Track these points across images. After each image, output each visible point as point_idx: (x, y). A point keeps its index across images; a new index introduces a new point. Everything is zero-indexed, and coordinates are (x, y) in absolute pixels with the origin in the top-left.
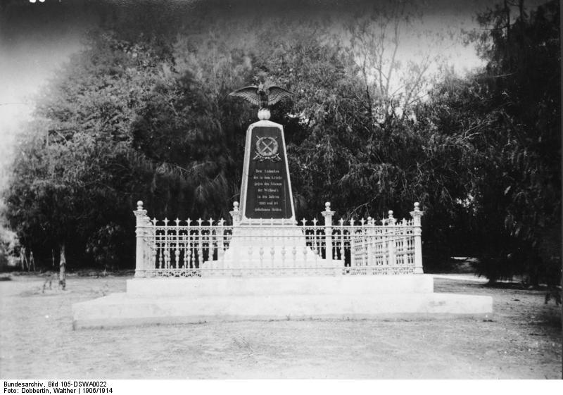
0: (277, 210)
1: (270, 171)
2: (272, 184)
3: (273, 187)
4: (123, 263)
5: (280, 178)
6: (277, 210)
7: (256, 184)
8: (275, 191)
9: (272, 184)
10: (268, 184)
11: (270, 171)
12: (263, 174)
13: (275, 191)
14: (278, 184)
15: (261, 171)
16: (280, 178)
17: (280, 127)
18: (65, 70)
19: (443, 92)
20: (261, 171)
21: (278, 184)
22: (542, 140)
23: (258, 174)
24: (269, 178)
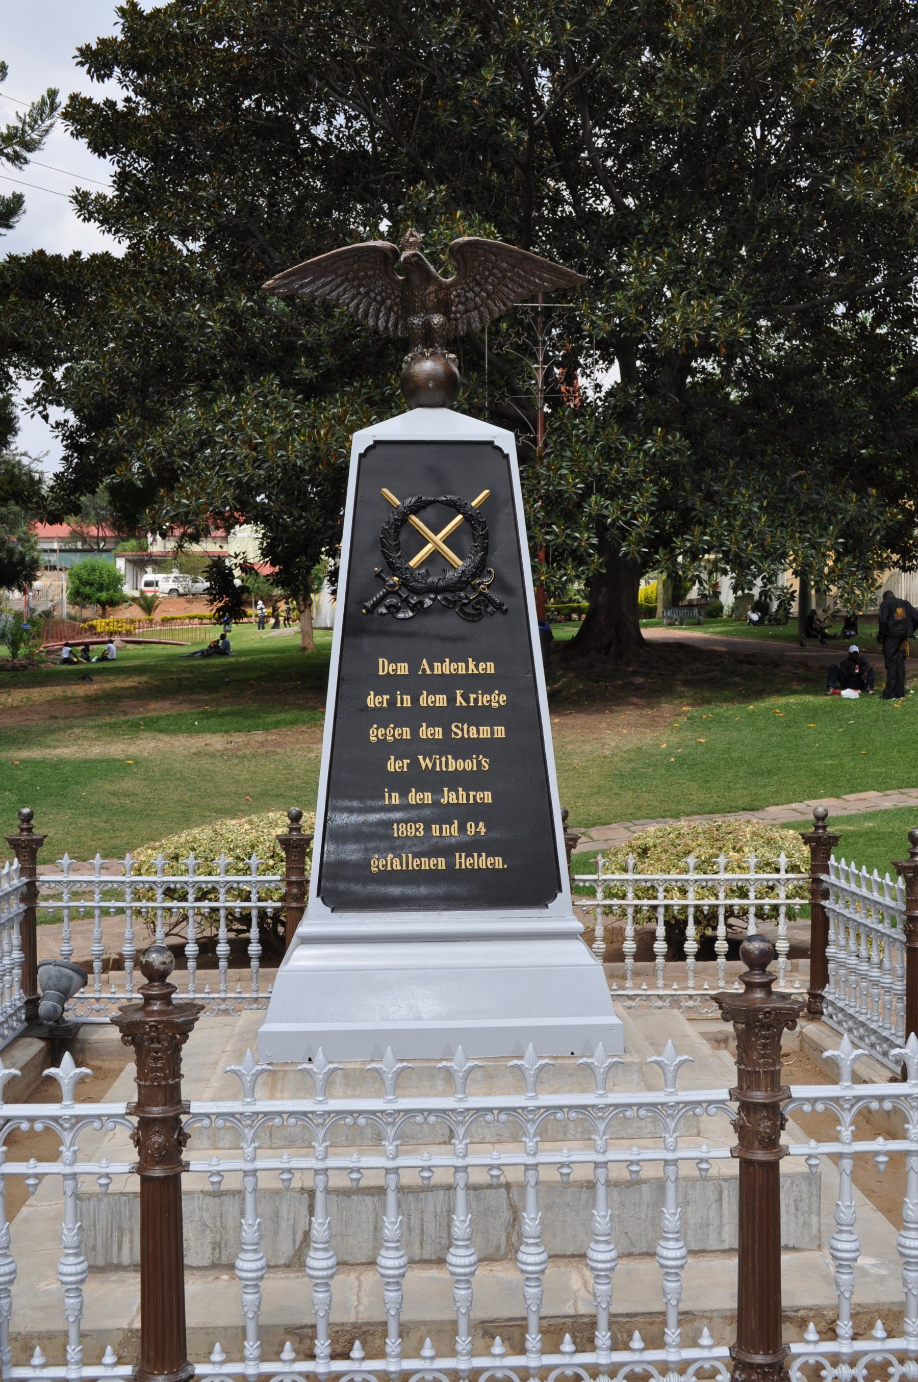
0: (483, 862)
1: (445, 668)
2: (460, 731)
3: (464, 749)
4: (74, 98)
5: (498, 699)
6: (483, 862)
7: (375, 734)
8: (469, 765)
9: (460, 731)
10: (439, 733)
11: (445, 668)
12: (415, 683)
13: (469, 765)
14: (485, 732)
15: (403, 669)
16: (498, 699)
17: (506, 440)
18: (729, 1027)
19: (78, 604)
20: (403, 669)
21: (485, 732)
22: (431, 377)
23: (390, 684)
24: (441, 700)
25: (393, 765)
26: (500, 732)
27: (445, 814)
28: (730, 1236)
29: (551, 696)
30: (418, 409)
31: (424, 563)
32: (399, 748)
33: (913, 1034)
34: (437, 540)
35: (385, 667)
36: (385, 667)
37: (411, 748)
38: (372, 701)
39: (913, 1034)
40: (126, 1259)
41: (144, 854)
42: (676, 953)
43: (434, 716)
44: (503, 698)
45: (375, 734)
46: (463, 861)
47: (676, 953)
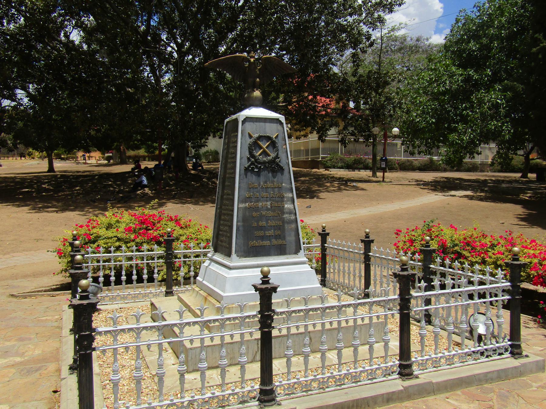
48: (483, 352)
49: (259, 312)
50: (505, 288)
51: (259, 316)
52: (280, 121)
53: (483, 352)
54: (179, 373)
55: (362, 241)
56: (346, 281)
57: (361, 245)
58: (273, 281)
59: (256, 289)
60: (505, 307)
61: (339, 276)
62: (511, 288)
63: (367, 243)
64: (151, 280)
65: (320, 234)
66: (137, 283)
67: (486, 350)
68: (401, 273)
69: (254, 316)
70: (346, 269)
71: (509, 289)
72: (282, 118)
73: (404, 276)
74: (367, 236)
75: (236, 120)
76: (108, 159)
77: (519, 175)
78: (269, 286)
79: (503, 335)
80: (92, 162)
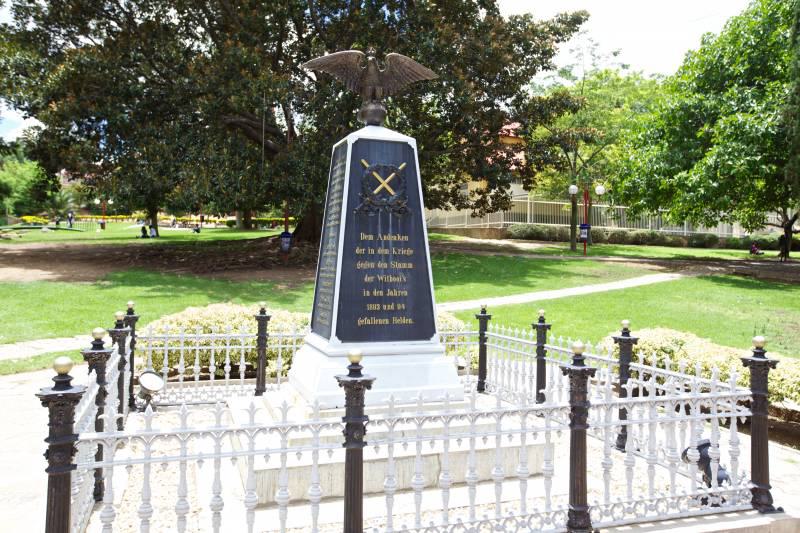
0: (404, 321)
5: (410, 252)
6: (404, 321)
16: (410, 252)
20: (371, 237)
23: (364, 244)
25: (368, 279)
26: (410, 266)
27: (378, 300)
28: (366, 468)
29: (431, 255)
30: (370, 127)
31: (379, 193)
32: (370, 272)
33: (94, 370)
34: (384, 183)
35: (363, 236)
36: (363, 236)
37: (374, 272)
38: (358, 251)
39: (94, 370)
40: (368, 464)
41: (167, 318)
42: (205, 361)
43: (387, 258)
44: (411, 252)
45: (360, 265)
46: (396, 321)
47: (205, 361)
48: (707, 499)
49: (344, 418)
50: (742, 400)
51: (344, 424)
52: (410, 146)
53: (707, 499)
54: (247, 506)
55: (535, 327)
56: (499, 380)
57: (533, 333)
58: (367, 373)
59: (342, 384)
60: (741, 427)
61: (503, 378)
62: (752, 400)
63: (542, 329)
64: (235, 374)
65: (478, 317)
66: (231, 377)
67: (711, 495)
68: (573, 368)
69: (336, 425)
70: (520, 368)
71: (748, 401)
72: (412, 142)
73: (576, 372)
74: (542, 320)
75: (345, 143)
76: (230, 224)
77: (777, 253)
78: (359, 379)
79: (740, 473)
80: (212, 227)
